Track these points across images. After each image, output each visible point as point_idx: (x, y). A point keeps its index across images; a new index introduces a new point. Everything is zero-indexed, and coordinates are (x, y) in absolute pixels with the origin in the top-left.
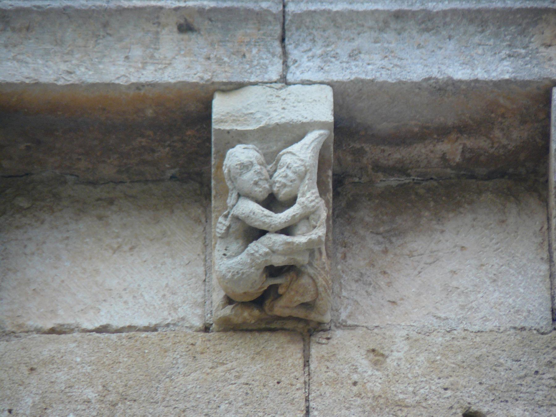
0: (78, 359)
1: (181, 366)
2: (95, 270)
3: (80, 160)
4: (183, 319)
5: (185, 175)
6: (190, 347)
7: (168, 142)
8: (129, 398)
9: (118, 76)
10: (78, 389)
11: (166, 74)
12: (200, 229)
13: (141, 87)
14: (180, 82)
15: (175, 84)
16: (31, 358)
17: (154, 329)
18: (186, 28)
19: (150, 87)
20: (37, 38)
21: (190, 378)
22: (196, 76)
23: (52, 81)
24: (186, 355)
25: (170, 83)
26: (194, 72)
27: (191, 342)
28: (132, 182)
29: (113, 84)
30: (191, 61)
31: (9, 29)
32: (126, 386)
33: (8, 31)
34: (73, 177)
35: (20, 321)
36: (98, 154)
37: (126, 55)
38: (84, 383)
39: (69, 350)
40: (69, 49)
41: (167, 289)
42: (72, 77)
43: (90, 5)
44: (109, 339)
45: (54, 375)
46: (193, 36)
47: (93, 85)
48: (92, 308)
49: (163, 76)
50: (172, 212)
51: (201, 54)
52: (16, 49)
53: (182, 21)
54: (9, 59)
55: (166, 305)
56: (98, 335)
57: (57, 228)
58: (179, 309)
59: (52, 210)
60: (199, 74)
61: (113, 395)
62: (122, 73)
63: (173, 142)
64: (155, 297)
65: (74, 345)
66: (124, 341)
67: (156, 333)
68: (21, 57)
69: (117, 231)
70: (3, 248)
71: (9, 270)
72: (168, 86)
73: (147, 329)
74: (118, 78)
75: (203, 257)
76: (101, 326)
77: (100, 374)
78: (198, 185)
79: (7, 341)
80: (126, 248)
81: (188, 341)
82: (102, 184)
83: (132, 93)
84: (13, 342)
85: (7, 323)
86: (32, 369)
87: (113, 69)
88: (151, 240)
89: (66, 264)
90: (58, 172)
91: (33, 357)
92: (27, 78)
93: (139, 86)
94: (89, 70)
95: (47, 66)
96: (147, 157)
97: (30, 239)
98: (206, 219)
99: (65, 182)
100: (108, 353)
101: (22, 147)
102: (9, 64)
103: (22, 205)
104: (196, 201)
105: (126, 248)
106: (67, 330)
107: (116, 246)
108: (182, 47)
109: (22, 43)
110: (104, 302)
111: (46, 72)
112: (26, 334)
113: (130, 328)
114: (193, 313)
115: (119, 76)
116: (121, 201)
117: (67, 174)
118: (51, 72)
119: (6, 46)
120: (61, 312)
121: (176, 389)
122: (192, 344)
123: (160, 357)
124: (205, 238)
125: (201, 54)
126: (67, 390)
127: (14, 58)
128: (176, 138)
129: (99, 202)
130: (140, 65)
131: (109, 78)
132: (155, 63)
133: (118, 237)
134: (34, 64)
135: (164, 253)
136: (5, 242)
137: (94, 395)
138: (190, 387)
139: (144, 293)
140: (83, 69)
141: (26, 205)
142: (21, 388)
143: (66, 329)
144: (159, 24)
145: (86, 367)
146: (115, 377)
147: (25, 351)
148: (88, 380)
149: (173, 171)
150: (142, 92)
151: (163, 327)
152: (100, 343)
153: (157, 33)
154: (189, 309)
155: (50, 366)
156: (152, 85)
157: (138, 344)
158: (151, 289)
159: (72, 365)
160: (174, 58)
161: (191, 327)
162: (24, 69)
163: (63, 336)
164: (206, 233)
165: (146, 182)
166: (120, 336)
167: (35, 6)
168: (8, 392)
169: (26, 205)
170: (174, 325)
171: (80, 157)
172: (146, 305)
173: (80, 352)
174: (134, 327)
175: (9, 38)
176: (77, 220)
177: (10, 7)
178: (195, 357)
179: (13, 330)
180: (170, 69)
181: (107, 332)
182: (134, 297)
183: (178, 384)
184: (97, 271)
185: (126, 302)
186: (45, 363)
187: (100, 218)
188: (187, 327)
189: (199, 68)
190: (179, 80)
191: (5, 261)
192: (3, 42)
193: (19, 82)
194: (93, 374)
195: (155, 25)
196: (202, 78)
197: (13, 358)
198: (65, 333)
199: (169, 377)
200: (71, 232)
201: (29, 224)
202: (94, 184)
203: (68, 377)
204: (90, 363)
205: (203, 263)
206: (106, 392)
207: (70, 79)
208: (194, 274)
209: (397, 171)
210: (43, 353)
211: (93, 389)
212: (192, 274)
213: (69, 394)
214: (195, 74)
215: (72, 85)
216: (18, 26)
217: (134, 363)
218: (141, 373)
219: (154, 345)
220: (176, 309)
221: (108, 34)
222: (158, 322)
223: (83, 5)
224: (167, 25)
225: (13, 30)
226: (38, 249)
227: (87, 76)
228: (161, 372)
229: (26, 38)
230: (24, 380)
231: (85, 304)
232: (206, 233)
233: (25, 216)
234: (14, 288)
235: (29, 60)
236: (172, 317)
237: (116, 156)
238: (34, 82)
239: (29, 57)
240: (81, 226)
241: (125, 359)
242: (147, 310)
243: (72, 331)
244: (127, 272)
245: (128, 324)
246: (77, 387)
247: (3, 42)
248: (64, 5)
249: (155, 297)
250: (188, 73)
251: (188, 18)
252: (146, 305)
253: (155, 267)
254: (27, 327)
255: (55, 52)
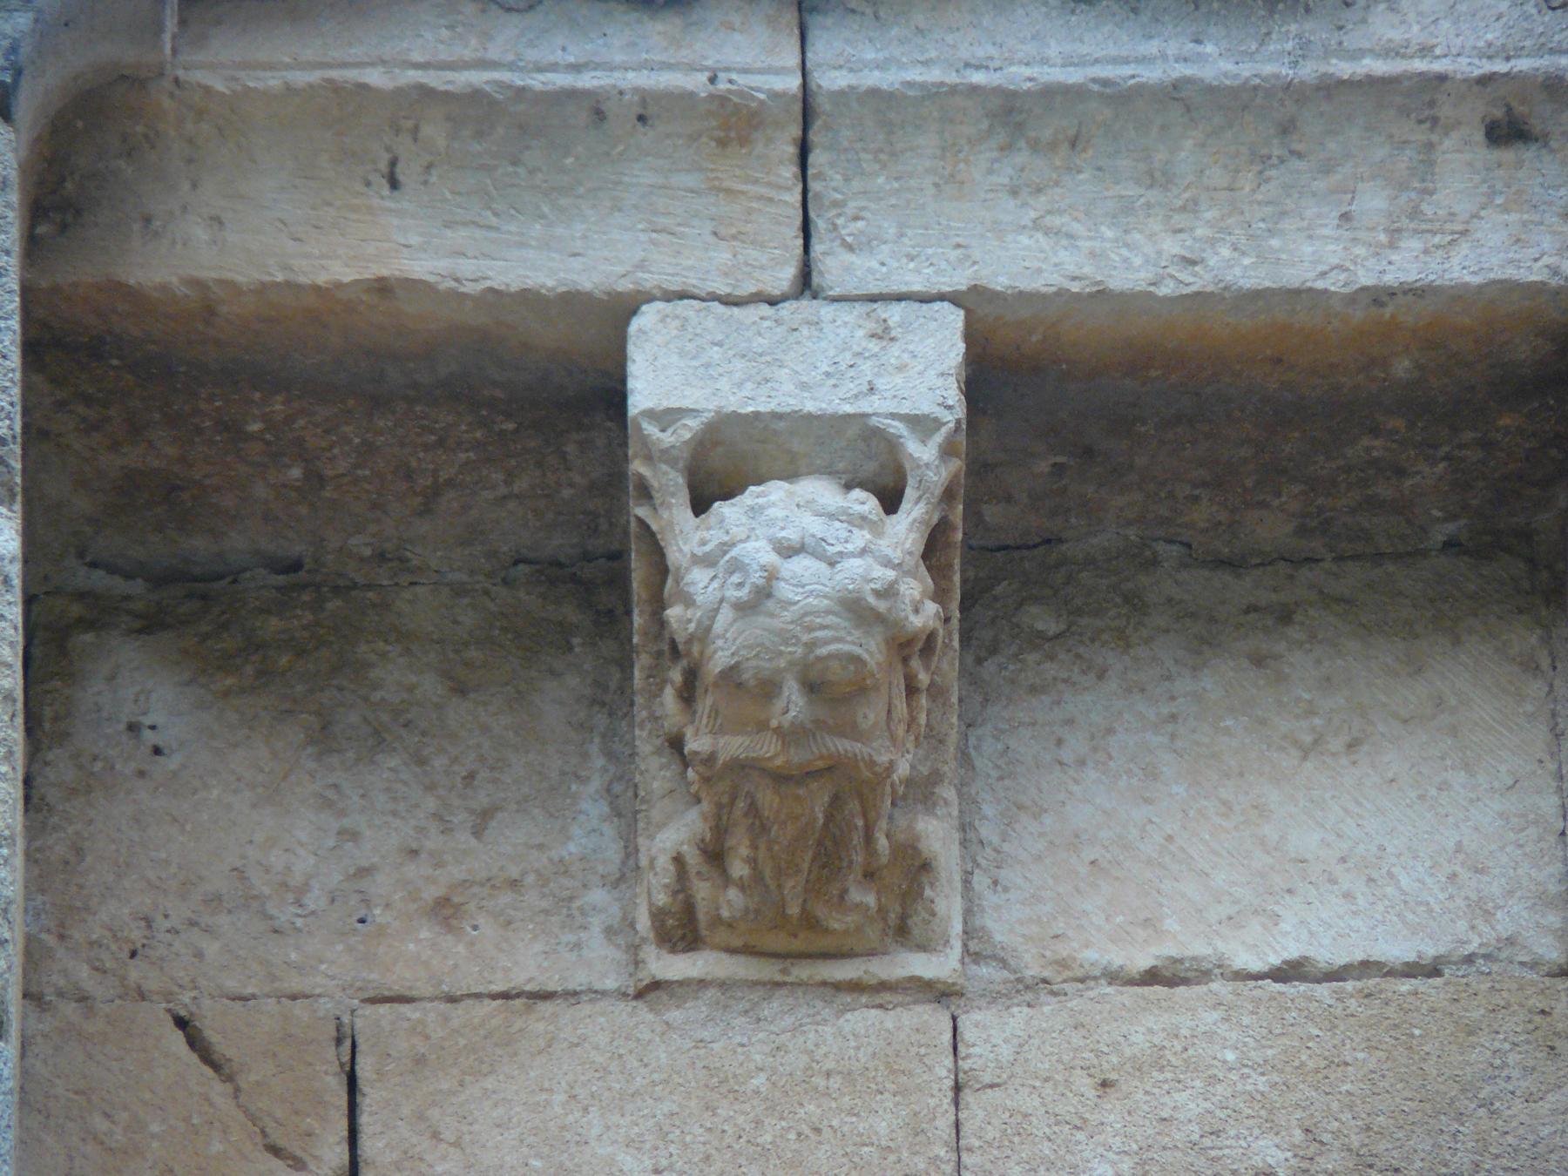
0: (1230, 1056)
1: (1516, 1074)
2: (1256, 807)
3: (1196, 499)
4: (1511, 941)
5: (1488, 538)
6: (1538, 1019)
7: (1446, 449)
8: (1379, 1164)
9: (1321, 268)
10: (1238, 1137)
11: (1455, 261)
12: (1537, 687)
13: (1385, 299)
14: (1494, 282)
15: (1481, 288)
16: (1099, 1054)
17: (1432, 970)
18: (1508, 132)
19: (1410, 297)
20: (1100, 169)
21: (1544, 1107)
22: (1540, 263)
23: (1142, 286)
24: (1528, 1042)
25: (1466, 285)
26: (1534, 252)
27: (1540, 1006)
28: (1340, 559)
29: (1310, 290)
30: (1524, 224)
31: (1022, 144)
32: (1368, 1128)
33: (1020, 150)
34: (1175, 547)
35: (1063, 950)
36: (1249, 483)
37: (1345, 209)
38: (1251, 1122)
39: (1202, 1028)
40: (1187, 195)
41: (1461, 857)
42: (1195, 275)
43: (1246, 74)
44: (1310, 999)
45: (1166, 1099)
46: (1529, 153)
47: (1257, 295)
48: (1256, 912)
49: (1447, 266)
50: (1457, 641)
51: (1550, 204)
52: (1043, 199)
53: (1499, 113)
54: (1024, 227)
55: (1460, 902)
56: (1279, 987)
57: (1143, 690)
58: (1499, 915)
59: (1123, 640)
60: (1546, 260)
61: (1335, 1156)
62: (1335, 261)
63: (1461, 447)
64: (1429, 880)
65: (1216, 1015)
66: (1353, 1004)
67: (1438, 981)
68: (1056, 221)
69: (1306, 696)
70: (1000, 746)
71: (1020, 807)
72: (1459, 295)
73: (1411, 970)
74: (1323, 274)
75: (1552, 767)
76: (1285, 962)
77: (1294, 1097)
78: (1521, 565)
79: (1029, 1005)
80: (1336, 744)
81: (1530, 1002)
82: (1257, 566)
83: (1358, 315)
84: (1046, 1009)
85: (1027, 957)
86: (1105, 1084)
87: (1308, 249)
88: (1405, 721)
89: (1175, 789)
90: (1132, 534)
91: (1105, 1049)
92: (1074, 279)
93: (1378, 296)
94: (1244, 253)
95: (1127, 245)
96: (1384, 490)
97: (1070, 722)
98: (1553, 661)
99: (1155, 562)
100: (1310, 1038)
101: (1043, 467)
102: (1024, 240)
103: (1040, 626)
104: (1521, 612)
105: (1336, 744)
106: (1190, 974)
107: (1308, 739)
108: (1499, 186)
109: (1057, 184)
110: (1287, 897)
111: (1126, 260)
112: (1081, 986)
113: (1367, 968)
114: (1538, 924)
115: (1326, 268)
116: (1311, 612)
117: (1156, 540)
118: (1138, 261)
119: (1014, 192)
120: (1171, 924)
121: (1510, 1139)
122: (1543, 1012)
123: (1454, 1047)
124: (1554, 714)
125: (1550, 204)
126: (1207, 1142)
127: (1036, 225)
128: (1468, 436)
129: (1253, 616)
130: (1383, 238)
131: (1295, 275)
132: (1423, 232)
133: (1311, 712)
134: (1090, 238)
135: (1443, 758)
136: (1002, 731)
137: (1281, 1156)
138: (1545, 1131)
139: (1394, 870)
140: (1225, 252)
141: (1050, 625)
142: (1080, 1136)
143: (1187, 970)
144: (1435, 121)
145: (1254, 1075)
146: (1335, 1106)
147: (1083, 1032)
148: (1263, 1113)
149: (1451, 528)
150: (1387, 312)
151: (1455, 963)
152: (1288, 1010)
153: (1430, 146)
154: (1525, 914)
155: (1155, 1074)
156: (1417, 292)
157: (1390, 1011)
158: (1415, 858)
159: (1216, 1071)
160: (1475, 216)
161: (1533, 965)
162: (1063, 255)
163: (1181, 990)
164: (1555, 700)
165: (1378, 557)
166: (1343, 990)
167: (1094, 80)
168: (1046, 1148)
169: (1050, 625)
170: (1487, 957)
171: (1197, 492)
172: (1406, 902)
173: (1234, 1035)
174: (1377, 963)
175: (1022, 170)
176: (1194, 669)
177: (1029, 84)
178: (1552, 1048)
179: (1046, 974)
180: (1464, 248)
181: (1304, 978)
182: (1371, 880)
183: (1514, 1124)
184: (1261, 810)
185: (1348, 896)
186: (1137, 1068)
187: (1259, 661)
188: (1522, 964)
189: (1547, 243)
190: (1492, 276)
191: (1007, 782)
192: (1006, 181)
193: (1053, 289)
194: (1274, 1095)
195: (1423, 126)
196: (1555, 272)
197: (1052, 1054)
198: (1185, 981)
199: (1486, 1104)
200: (1181, 700)
201: (1065, 681)
202: (1232, 564)
203: (1208, 1105)
204: (1264, 1067)
205: (1554, 784)
206: (1314, 1147)
207: (1192, 280)
208: (1532, 817)
209: (1156, 503)
210: (1133, 1039)
211: (1277, 1140)
212: (1524, 816)
213: (1213, 1153)
214: (1536, 260)
215: (1198, 294)
216: (1047, 134)
217: (1385, 1067)
218: (1407, 1094)
219: (1437, 1015)
220: (1488, 915)
221: (1292, 152)
222: (1442, 950)
223: (1226, 75)
224: (1458, 124)
225: (1035, 146)
226: (1095, 750)
227: (1237, 271)
228: (1463, 1091)
229: (1069, 169)
230: (1087, 1116)
231: (1236, 902)
232: (1555, 700)
233: (1051, 658)
234: (1039, 858)
235: (1076, 227)
236: (1480, 936)
237: (1296, 489)
238: (1095, 289)
239: (1076, 219)
240: (1208, 682)
241: (1361, 1055)
242: (1410, 917)
243: (1204, 976)
244: (1346, 811)
245: (1359, 956)
246: (1232, 1133)
247: (1006, 181)
248: (1175, 75)
249: (1429, 880)
250: (1517, 256)
251: (1514, 104)
252: (1406, 902)
253: (1421, 797)
254: (1081, 966)
255: (1149, 205)
